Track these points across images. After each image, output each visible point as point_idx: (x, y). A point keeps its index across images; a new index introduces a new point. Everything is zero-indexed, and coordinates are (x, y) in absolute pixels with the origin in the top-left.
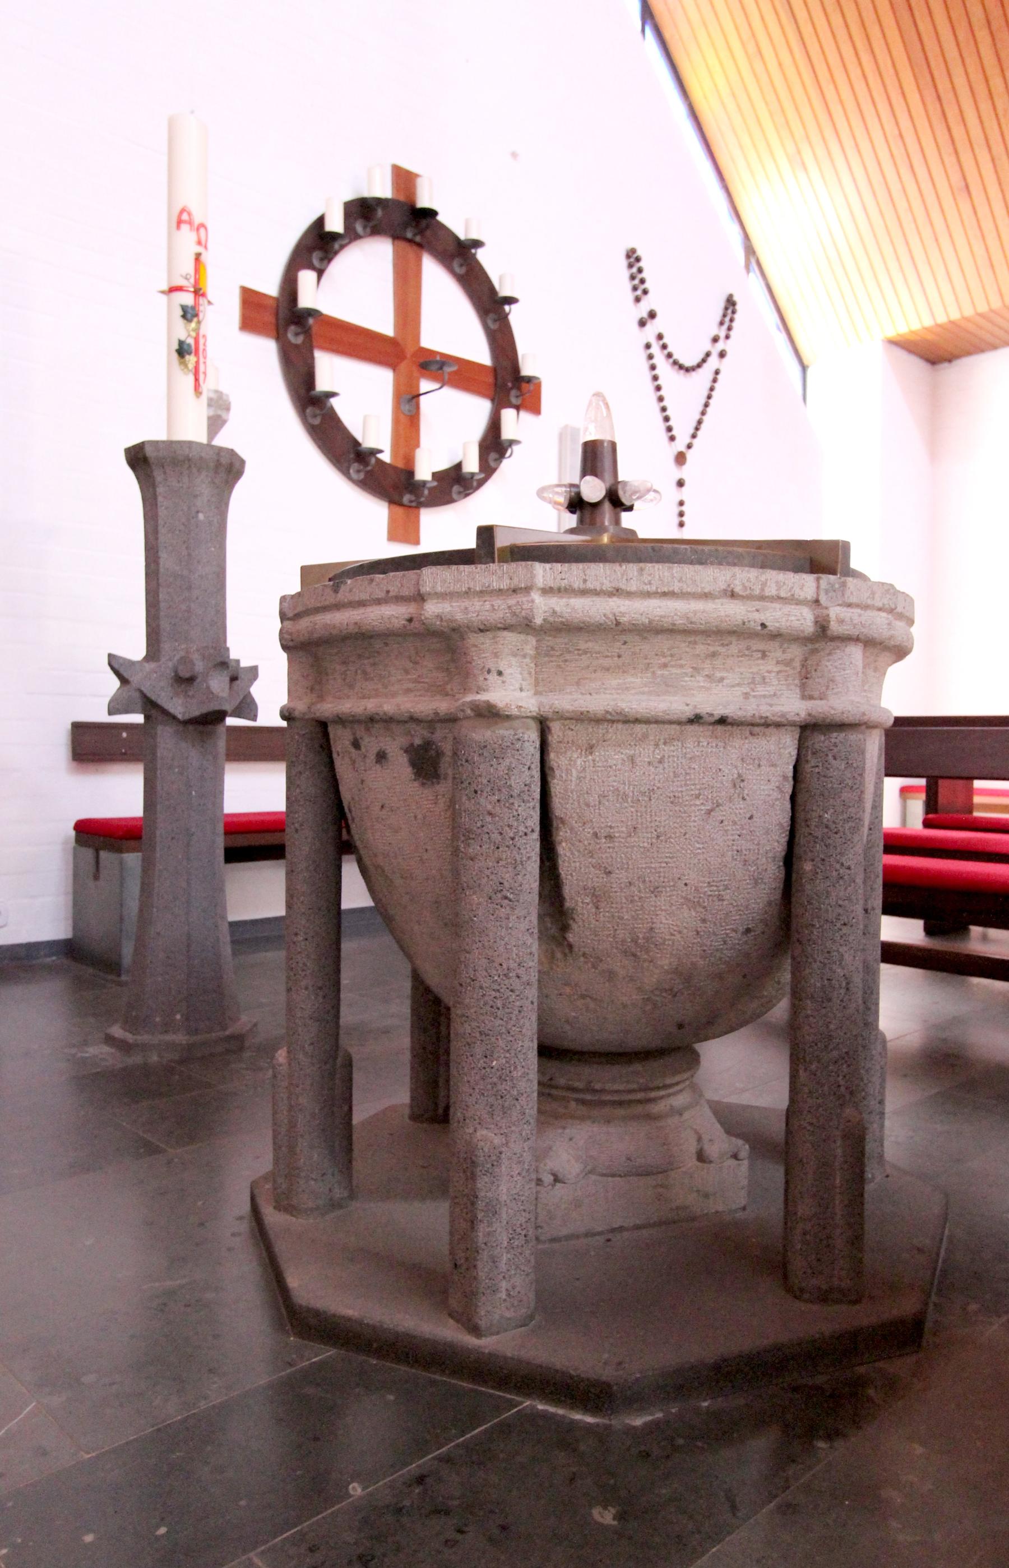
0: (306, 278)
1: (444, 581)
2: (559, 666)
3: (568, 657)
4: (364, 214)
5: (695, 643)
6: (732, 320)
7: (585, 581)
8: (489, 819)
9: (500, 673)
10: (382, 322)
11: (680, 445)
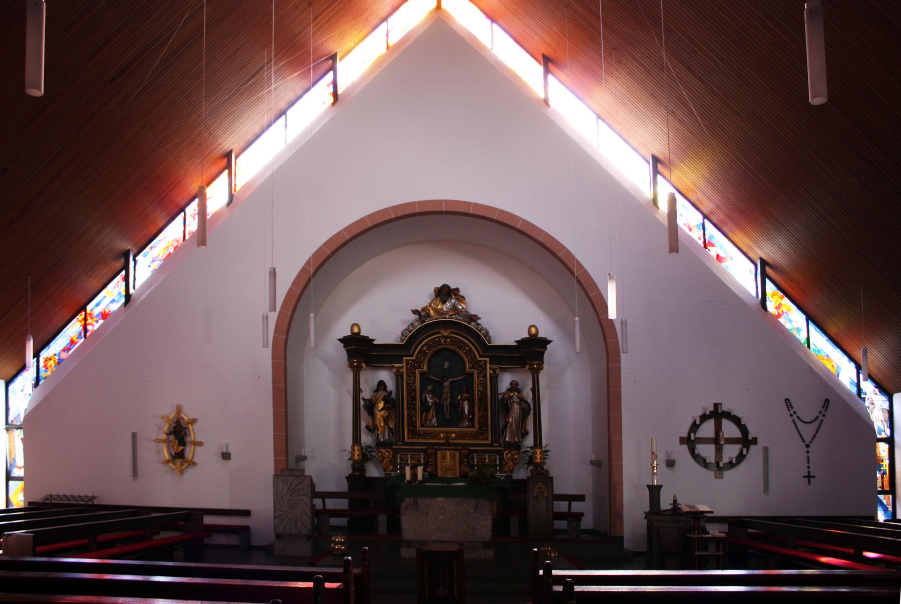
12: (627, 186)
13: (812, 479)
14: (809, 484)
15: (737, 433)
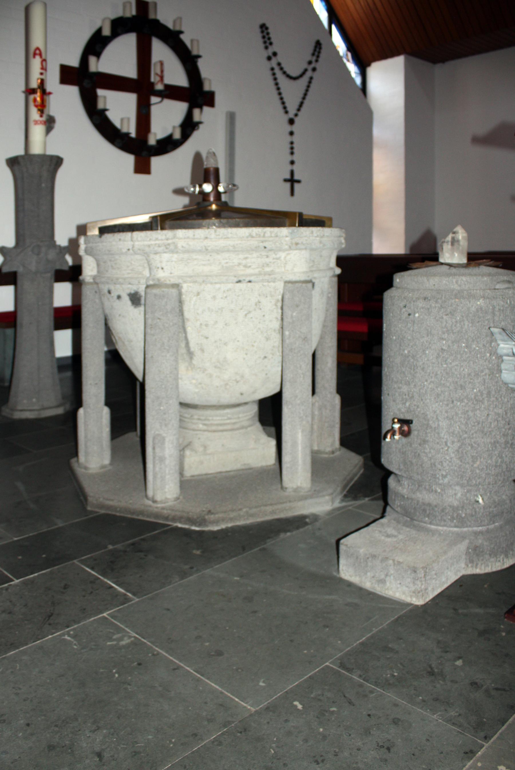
0: (92, 60)
1: (141, 237)
2: (186, 265)
3: (189, 261)
4: (120, 26)
5: (238, 254)
6: (319, 52)
7: (194, 235)
8: (158, 320)
9: (162, 269)
10: (130, 71)
11: (291, 115)
12: (395, 599)
13: (296, 185)
14: (292, 193)
15: (176, 76)
